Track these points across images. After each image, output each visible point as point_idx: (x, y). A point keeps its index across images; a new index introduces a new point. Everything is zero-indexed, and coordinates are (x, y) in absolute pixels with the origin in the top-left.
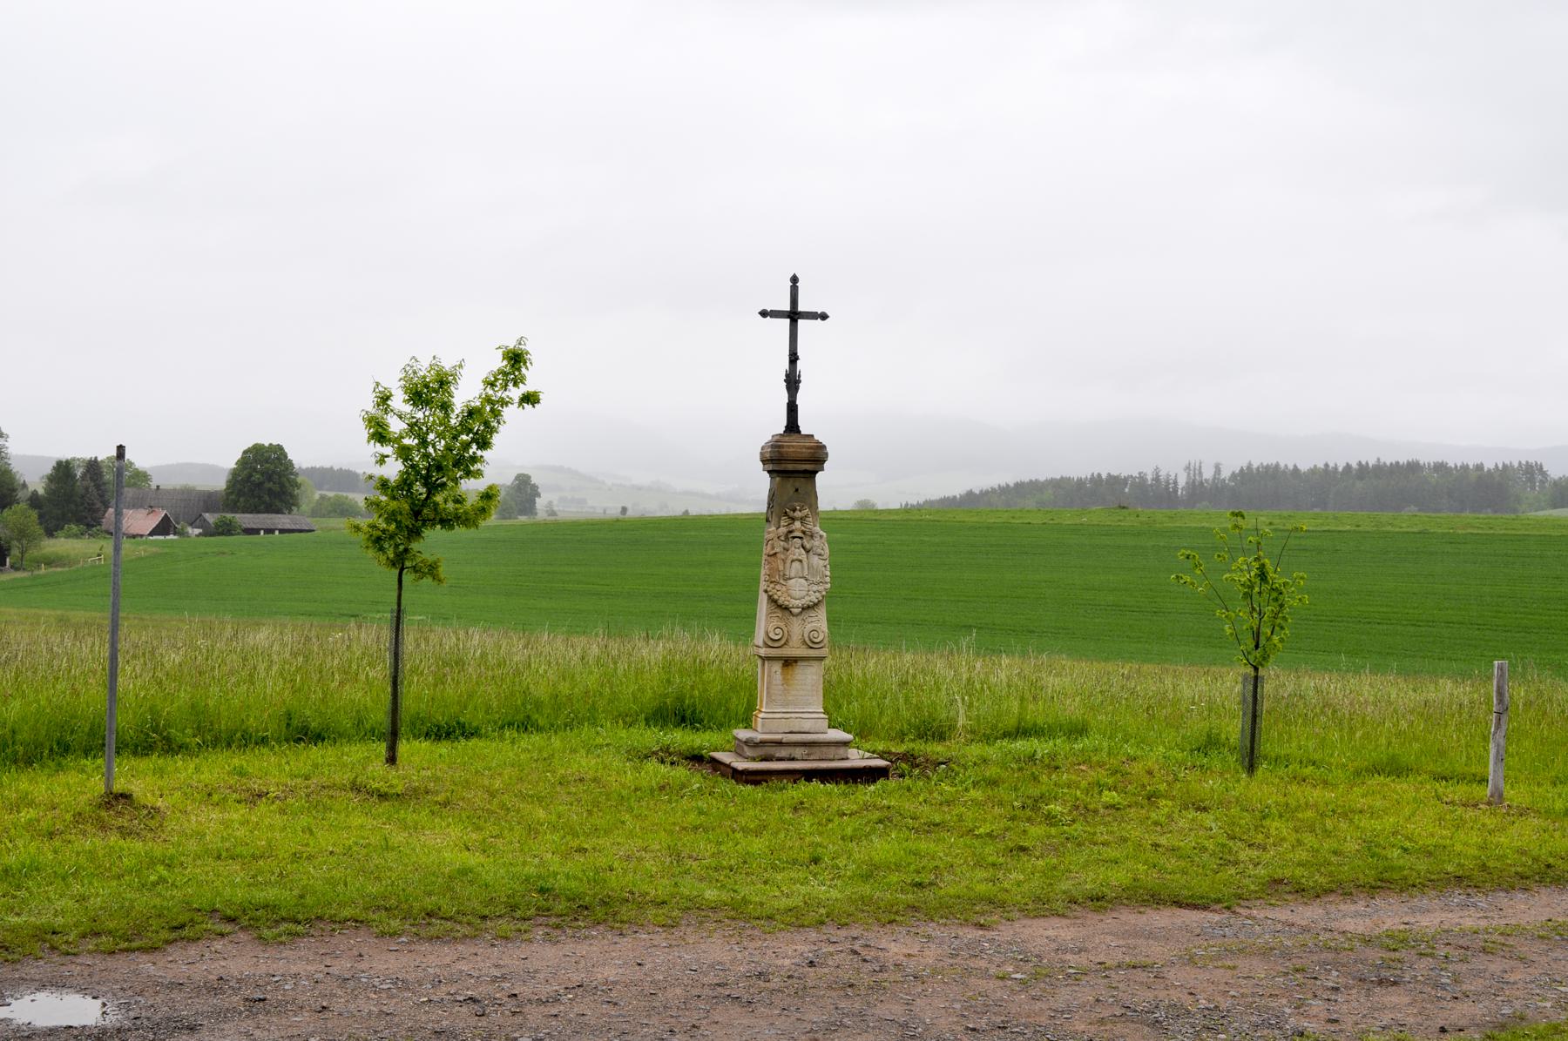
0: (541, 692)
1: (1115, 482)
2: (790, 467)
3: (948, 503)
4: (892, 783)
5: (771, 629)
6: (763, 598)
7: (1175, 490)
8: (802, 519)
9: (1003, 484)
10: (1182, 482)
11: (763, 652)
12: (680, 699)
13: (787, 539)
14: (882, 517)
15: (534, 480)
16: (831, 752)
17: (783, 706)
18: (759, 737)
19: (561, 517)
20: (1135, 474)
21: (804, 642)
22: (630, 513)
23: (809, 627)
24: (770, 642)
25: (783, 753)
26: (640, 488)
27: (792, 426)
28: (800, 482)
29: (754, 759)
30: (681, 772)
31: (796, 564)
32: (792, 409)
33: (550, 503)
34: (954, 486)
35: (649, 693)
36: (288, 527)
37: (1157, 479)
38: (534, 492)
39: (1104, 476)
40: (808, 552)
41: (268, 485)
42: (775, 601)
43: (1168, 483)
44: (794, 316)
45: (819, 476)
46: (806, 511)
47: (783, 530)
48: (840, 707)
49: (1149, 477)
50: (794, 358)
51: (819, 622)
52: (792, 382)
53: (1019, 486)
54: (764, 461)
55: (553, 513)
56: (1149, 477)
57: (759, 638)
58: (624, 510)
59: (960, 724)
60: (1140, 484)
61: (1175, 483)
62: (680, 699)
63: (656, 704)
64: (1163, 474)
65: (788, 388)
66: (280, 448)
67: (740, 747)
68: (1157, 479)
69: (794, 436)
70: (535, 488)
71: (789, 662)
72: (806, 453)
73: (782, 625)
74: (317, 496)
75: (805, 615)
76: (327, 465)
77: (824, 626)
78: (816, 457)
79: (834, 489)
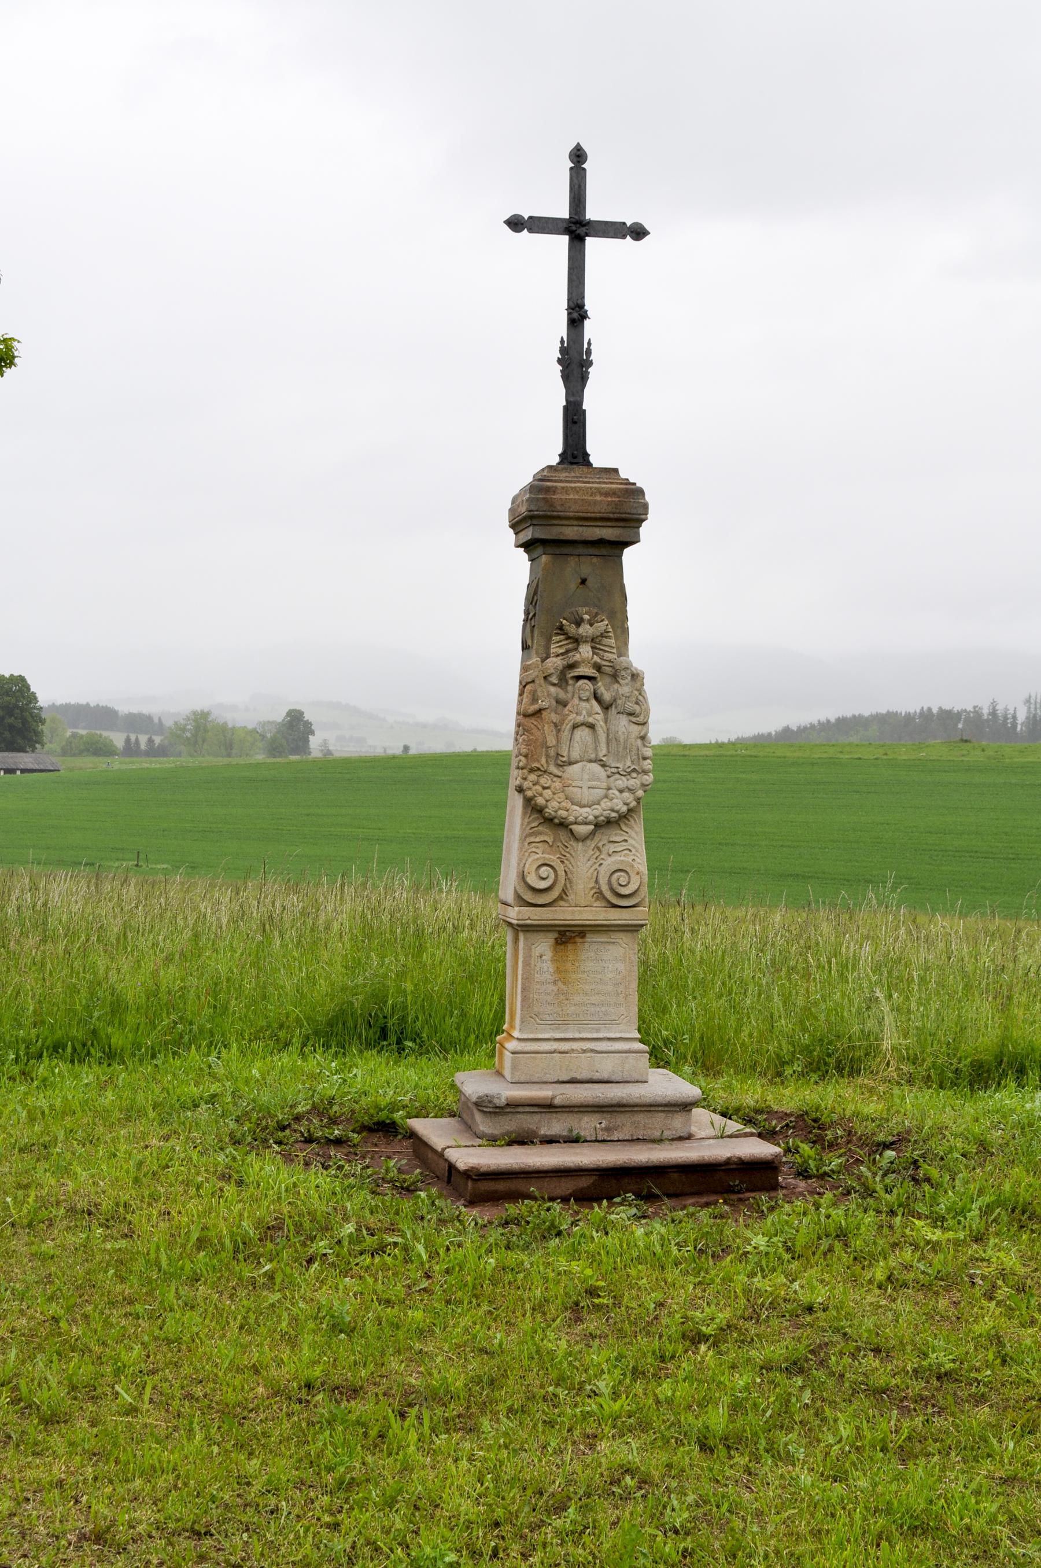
0: (132, 988)
1: (947, 717)
2: (570, 532)
3: (760, 741)
4: (795, 1216)
5: (530, 867)
6: (516, 802)
7: (1014, 725)
8: (595, 642)
9: (823, 719)
10: (1022, 716)
11: (514, 914)
12: (379, 998)
13: (563, 682)
14: (692, 753)
15: (307, 717)
16: (655, 1124)
17: (556, 1025)
18: (506, 1092)
19: (337, 755)
20: (970, 708)
21: (600, 895)
22: (413, 751)
23: (610, 863)
24: (530, 895)
25: (556, 1126)
26: (424, 726)
27: (575, 452)
28: (588, 566)
29: (493, 1141)
30: (315, 1185)
31: (582, 733)
32: (574, 419)
33: (325, 741)
34: (766, 721)
35: (323, 985)
36: (30, 766)
37: (994, 713)
38: (308, 729)
39: (935, 710)
40: (606, 707)
41: (11, 720)
42: (539, 810)
43: (1006, 718)
44: (577, 229)
45: (628, 553)
46: (602, 626)
47: (555, 663)
48: (665, 1010)
49: (985, 712)
50: (577, 315)
51: (631, 853)
52: (575, 364)
53: (842, 722)
54: (516, 525)
55: (329, 752)
56: (985, 712)
57: (508, 886)
58: (406, 748)
59: (886, 1044)
60: (974, 719)
61: (1014, 717)
62: (379, 998)
63: (331, 1007)
64: (1000, 708)
65: (566, 377)
66: (22, 679)
67: (463, 1112)
68: (994, 713)
69: (578, 471)
70: (308, 725)
71: (567, 936)
72: (602, 505)
73: (553, 858)
74: (68, 734)
75: (601, 839)
76: (83, 701)
77: (641, 863)
78: (621, 514)
79: (665, 593)
